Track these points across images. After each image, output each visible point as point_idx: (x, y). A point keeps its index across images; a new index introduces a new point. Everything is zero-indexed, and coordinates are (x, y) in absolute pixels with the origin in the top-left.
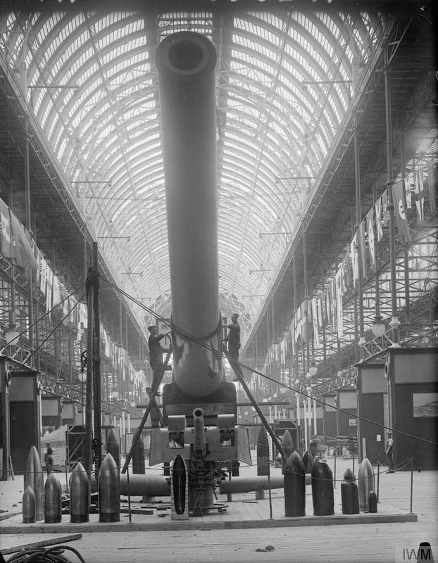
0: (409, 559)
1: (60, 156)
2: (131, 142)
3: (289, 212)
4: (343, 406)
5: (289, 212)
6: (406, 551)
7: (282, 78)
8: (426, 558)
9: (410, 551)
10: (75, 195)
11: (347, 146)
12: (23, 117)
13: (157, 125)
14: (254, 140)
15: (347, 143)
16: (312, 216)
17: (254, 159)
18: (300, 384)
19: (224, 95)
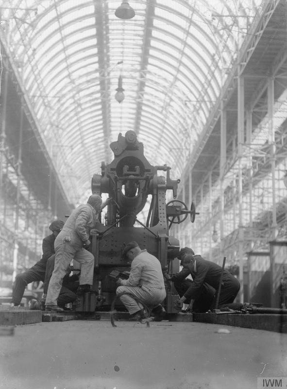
0: (267, 386)
1: (39, 116)
2: (83, 110)
7: (180, 76)
8: (278, 386)
14: (161, 113)
17: (161, 124)
18: (6, 254)
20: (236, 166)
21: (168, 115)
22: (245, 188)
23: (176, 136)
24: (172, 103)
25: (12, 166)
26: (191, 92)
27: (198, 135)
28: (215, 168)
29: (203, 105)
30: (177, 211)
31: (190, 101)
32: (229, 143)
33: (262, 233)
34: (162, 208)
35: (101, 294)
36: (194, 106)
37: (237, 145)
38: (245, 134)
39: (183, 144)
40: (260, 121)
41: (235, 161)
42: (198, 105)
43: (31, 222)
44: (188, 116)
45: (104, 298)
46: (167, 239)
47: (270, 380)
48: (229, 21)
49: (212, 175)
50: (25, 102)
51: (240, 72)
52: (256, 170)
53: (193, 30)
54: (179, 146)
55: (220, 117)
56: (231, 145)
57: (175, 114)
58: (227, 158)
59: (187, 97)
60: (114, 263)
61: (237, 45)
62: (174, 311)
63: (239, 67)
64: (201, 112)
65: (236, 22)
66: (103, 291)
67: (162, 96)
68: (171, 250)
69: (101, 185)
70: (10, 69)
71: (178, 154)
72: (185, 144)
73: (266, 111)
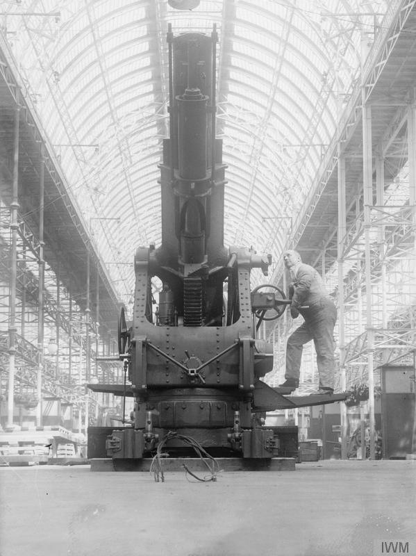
3: (281, 231)
4: (326, 412)
5: (281, 231)
6: (384, 544)
7: (275, 109)
8: (404, 551)
9: (388, 545)
11: (331, 171)
12: (40, 141)
13: (158, 150)
15: (353, 122)
16: (301, 235)
19: (224, 90)
20: (361, 240)
21: (260, 168)
22: (376, 273)
23: (272, 199)
24: (265, 151)
25: (31, 249)
26: (293, 132)
27: (305, 197)
28: (330, 245)
29: (311, 151)
30: (268, 301)
31: (291, 145)
32: (351, 207)
33: (401, 338)
34: (244, 296)
35: (152, 431)
36: (298, 153)
37: (362, 209)
38: (374, 192)
39: (282, 212)
40: (396, 172)
41: (361, 234)
42: (303, 151)
43: (62, 331)
44: (289, 169)
45: (157, 436)
46: (252, 344)
47: (391, 543)
48: (346, 23)
49: (326, 256)
50: (47, 155)
51: (364, 100)
52: (392, 246)
53: (293, 39)
54: (276, 213)
55: (336, 168)
56: (354, 209)
57: (270, 166)
58: (347, 229)
59: (287, 140)
60: (171, 383)
62: (267, 455)
63: (363, 92)
64: (308, 162)
65: (358, 24)
66: (154, 427)
67: (250, 141)
68: (259, 360)
69: (149, 263)
70: (23, 105)
71: (275, 225)
72: (285, 210)
73: (404, 156)
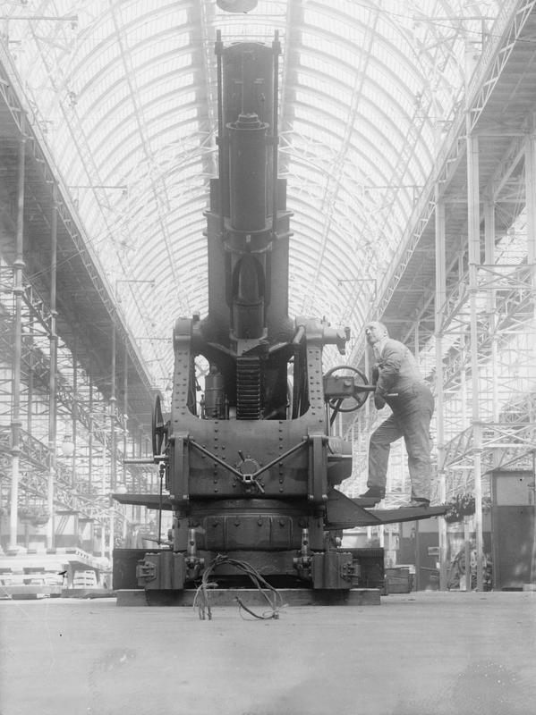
3: (362, 297)
5: (362, 297)
7: (355, 141)
10: (114, 294)
11: (427, 220)
12: (52, 182)
13: (204, 193)
15: (455, 157)
16: (388, 302)
19: (289, 116)
20: (465, 309)
21: (336, 216)
22: (485, 350)
23: (351, 255)
24: (341, 194)
25: (40, 321)
26: (377, 169)
27: (393, 254)
28: (426, 315)
29: (401, 194)
30: (346, 387)
31: (375, 186)
32: (452, 266)
33: (517, 434)
34: (314, 381)
35: (196, 555)
36: (384, 197)
37: (466, 269)
38: (482, 247)
39: (364, 272)
40: (511, 221)
41: (465, 301)
42: (391, 195)
43: (79, 425)
44: (372, 217)
45: (202, 560)
46: (325, 442)
48: (447, 30)
49: (420, 329)
50: (61, 199)
51: (469, 129)
52: (505, 316)
53: (378, 50)
54: (356, 274)
55: (433, 215)
56: (456, 268)
57: (348, 214)
58: (448, 294)
59: (369, 180)
60: (221, 492)
61: (462, 74)
62: (344, 585)
63: (468, 118)
64: (396, 208)
65: (461, 30)
66: (198, 549)
67: (323, 181)
68: (333, 464)
69: (192, 339)
70: (30, 135)
71: (354, 290)
72: (367, 271)
73: (521, 201)
